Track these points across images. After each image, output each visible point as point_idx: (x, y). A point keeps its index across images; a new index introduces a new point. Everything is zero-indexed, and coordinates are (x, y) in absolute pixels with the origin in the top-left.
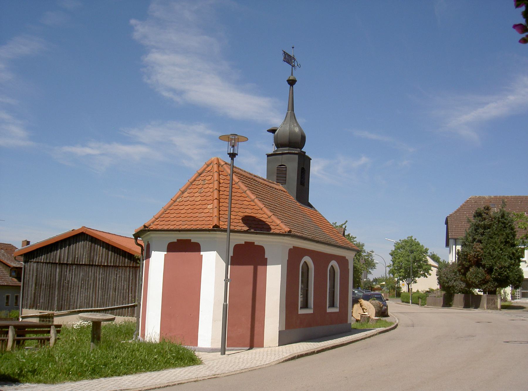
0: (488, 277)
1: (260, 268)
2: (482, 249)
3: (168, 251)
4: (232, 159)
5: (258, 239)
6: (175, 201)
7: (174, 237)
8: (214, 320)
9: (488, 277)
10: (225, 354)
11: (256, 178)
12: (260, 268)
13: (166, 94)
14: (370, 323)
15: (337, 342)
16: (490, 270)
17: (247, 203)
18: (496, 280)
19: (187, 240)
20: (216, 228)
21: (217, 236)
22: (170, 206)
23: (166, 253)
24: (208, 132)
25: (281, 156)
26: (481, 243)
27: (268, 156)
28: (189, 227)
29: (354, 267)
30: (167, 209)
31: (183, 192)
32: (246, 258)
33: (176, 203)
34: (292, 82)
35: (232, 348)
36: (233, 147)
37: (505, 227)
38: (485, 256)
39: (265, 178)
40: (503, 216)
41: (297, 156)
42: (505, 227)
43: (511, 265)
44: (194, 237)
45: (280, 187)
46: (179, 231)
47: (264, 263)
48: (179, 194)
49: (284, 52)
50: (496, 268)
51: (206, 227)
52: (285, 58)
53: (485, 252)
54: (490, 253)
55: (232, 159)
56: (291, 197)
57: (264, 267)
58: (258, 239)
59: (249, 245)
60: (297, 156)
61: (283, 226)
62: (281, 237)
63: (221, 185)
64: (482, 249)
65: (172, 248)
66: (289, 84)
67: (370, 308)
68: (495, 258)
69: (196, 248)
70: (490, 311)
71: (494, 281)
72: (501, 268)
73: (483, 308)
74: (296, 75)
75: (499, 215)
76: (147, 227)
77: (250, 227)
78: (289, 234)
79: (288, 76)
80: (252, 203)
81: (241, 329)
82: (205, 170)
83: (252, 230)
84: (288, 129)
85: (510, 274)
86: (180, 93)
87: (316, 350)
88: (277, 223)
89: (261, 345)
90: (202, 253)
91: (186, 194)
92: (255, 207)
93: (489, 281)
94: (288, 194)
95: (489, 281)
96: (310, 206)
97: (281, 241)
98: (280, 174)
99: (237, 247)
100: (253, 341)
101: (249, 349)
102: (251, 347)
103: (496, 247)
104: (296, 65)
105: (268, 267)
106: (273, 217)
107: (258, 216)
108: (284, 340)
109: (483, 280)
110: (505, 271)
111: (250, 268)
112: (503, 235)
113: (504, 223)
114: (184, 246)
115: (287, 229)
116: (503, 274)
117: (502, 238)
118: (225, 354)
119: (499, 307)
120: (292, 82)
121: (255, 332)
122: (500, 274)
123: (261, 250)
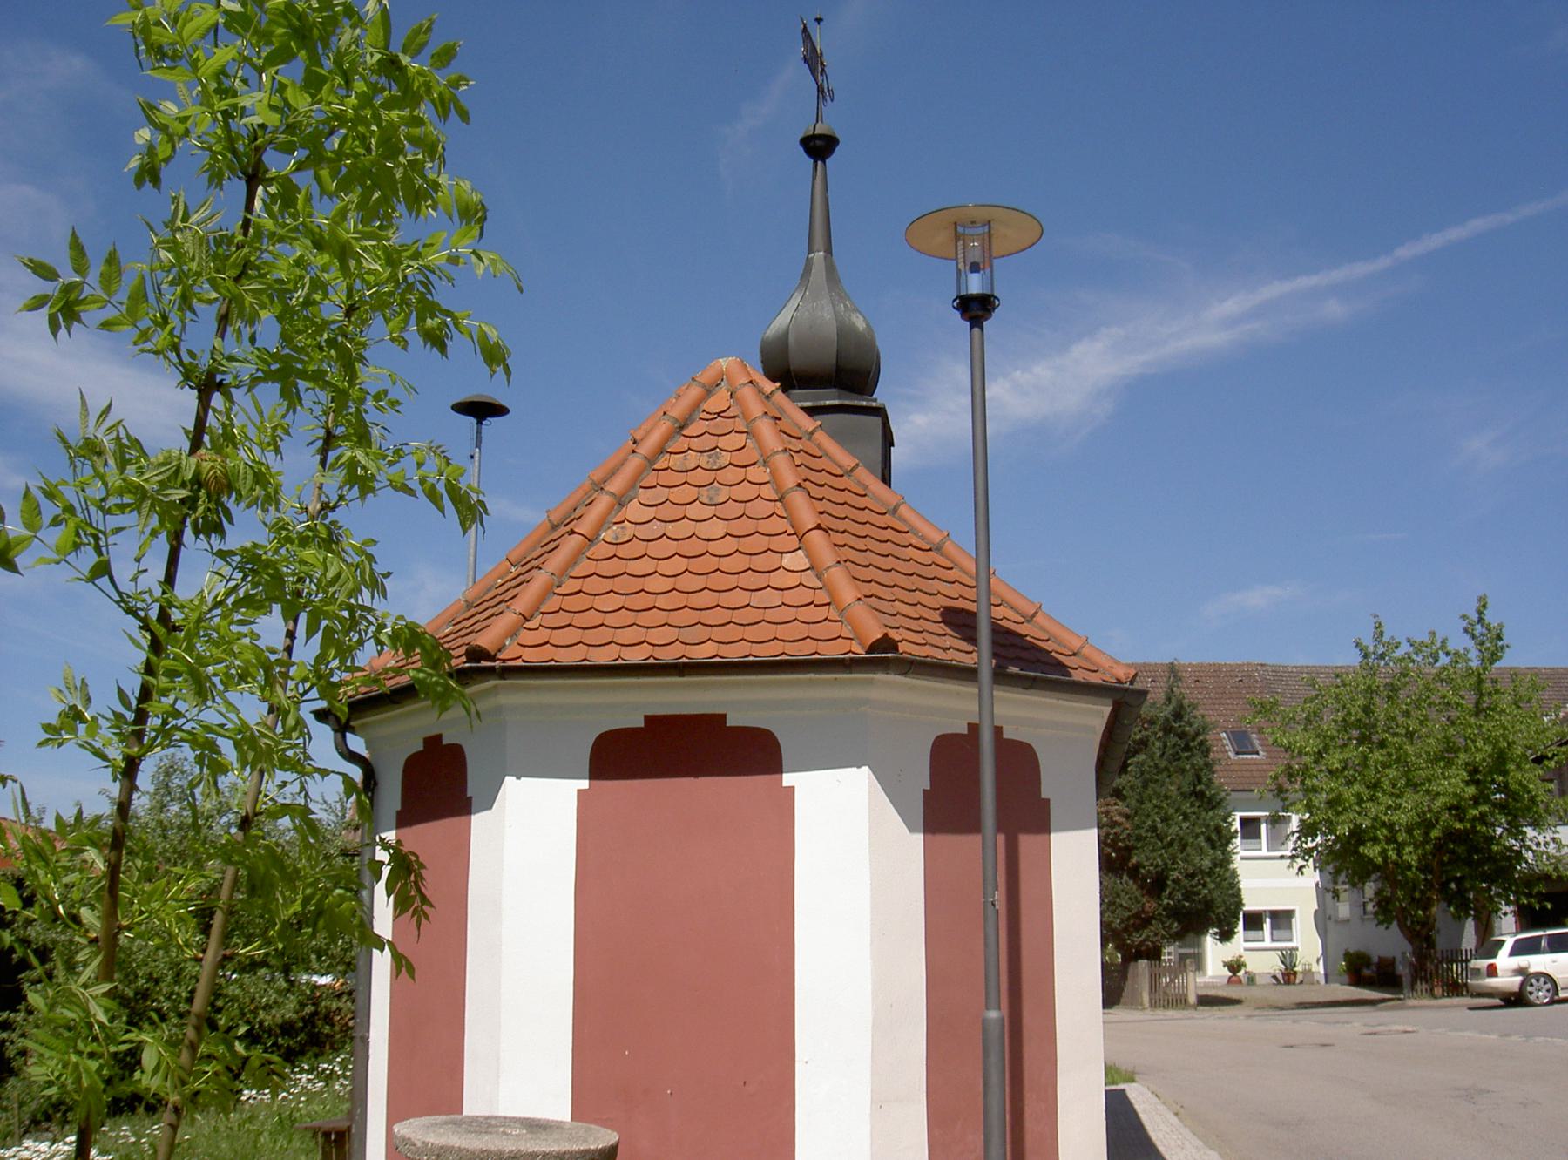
0: (1150, 905)
1: (1026, 841)
2: (1127, 817)
3: (594, 775)
7: (629, 706)
8: (879, 1103)
9: (1150, 905)
12: (1026, 841)
16: (1157, 885)
18: (1175, 913)
19: (696, 716)
20: (883, 656)
21: (875, 694)
23: (584, 784)
26: (1124, 798)
29: (208, 936)
33: (600, 550)
34: (819, 147)
37: (1187, 748)
38: (1139, 838)
40: (1178, 715)
42: (1187, 748)
43: (1215, 865)
44: (740, 703)
50: (1175, 874)
51: (832, 651)
53: (1138, 827)
54: (1154, 829)
57: (1040, 838)
64: (1127, 817)
65: (616, 757)
68: (1171, 844)
69: (757, 753)
70: (1160, 1012)
71: (1168, 917)
72: (1191, 876)
73: (1135, 1004)
75: (1167, 712)
76: (493, 659)
85: (1216, 894)
90: (788, 779)
91: (634, 510)
93: (1153, 918)
95: (1153, 918)
103: (1171, 811)
105: (1055, 837)
109: (1136, 916)
110: (1204, 886)
112: (1183, 771)
113: (1182, 735)
114: (685, 747)
116: (1198, 894)
117: (1185, 782)
119: (1192, 999)
120: (819, 147)
122: (1187, 897)
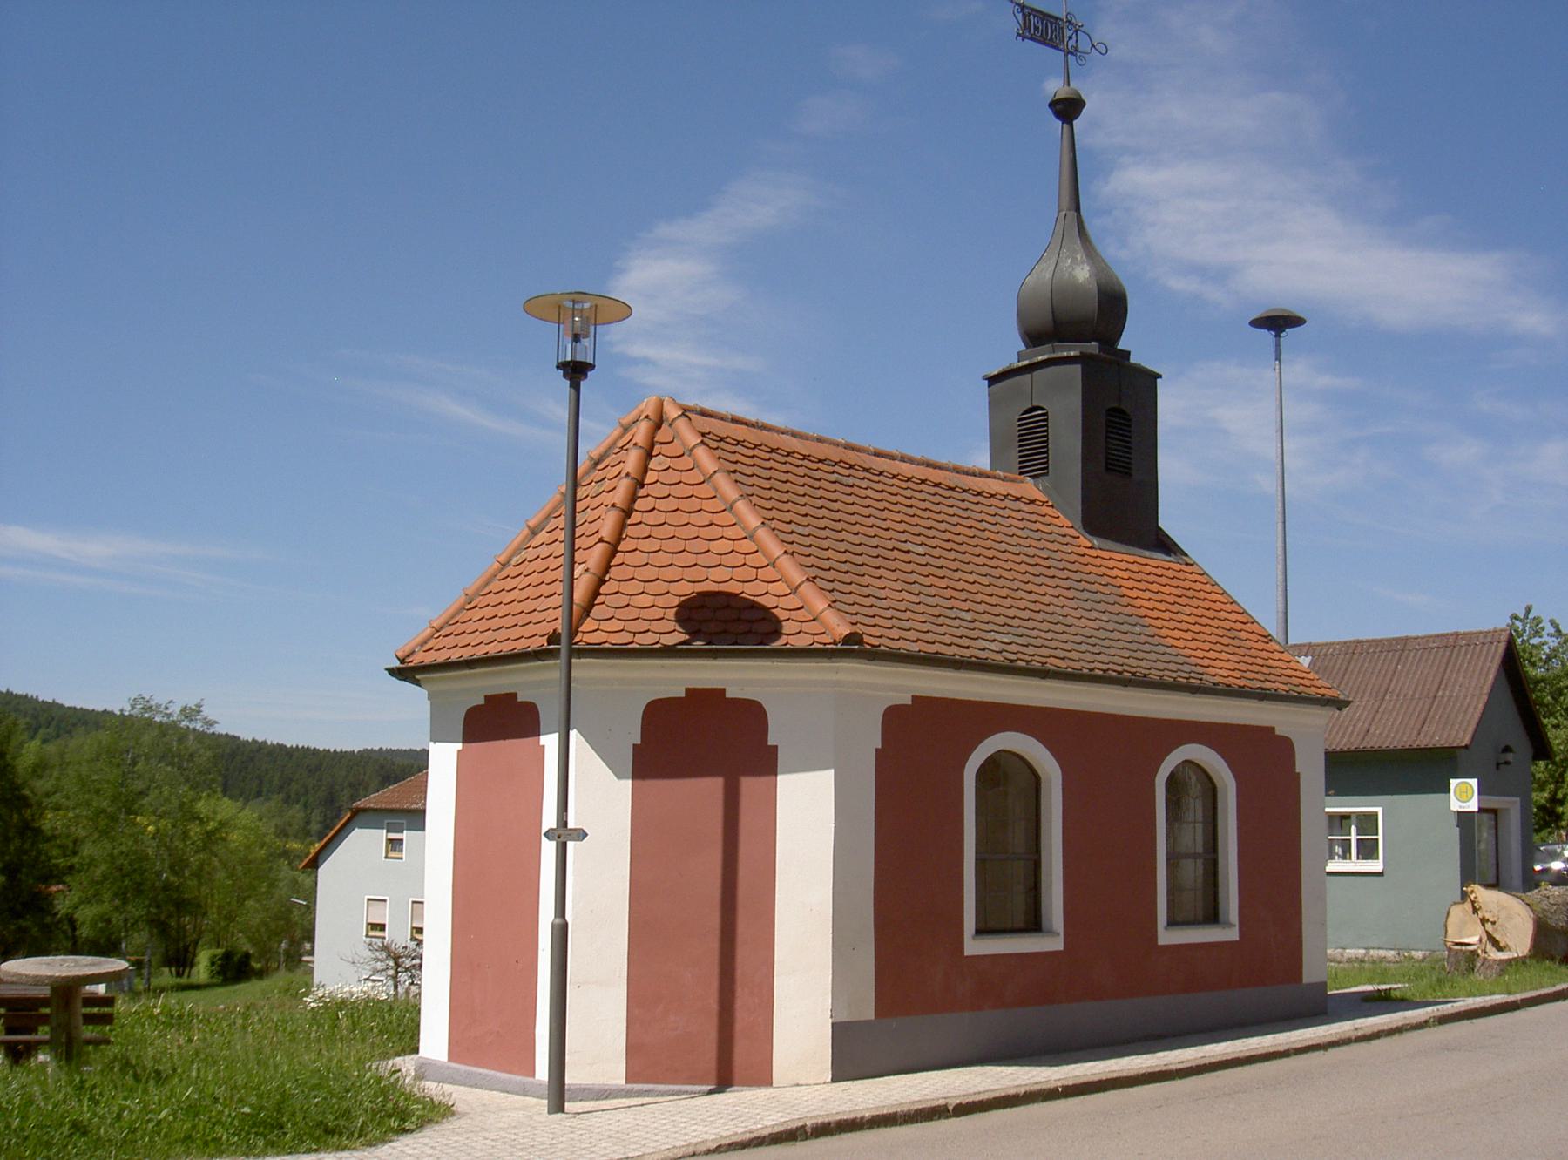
1: (748, 784)
4: (575, 386)
5: (736, 677)
6: (504, 566)
10: (562, 1110)
11: (852, 457)
12: (748, 784)
13: (1178, 284)
14: (1478, 976)
15: (1115, 1068)
17: (728, 546)
22: (487, 583)
23: (459, 746)
24: (1324, 381)
25: (1028, 376)
27: (993, 380)
28: (506, 648)
30: (477, 594)
31: (534, 532)
32: (701, 749)
35: (651, 1086)
36: (576, 338)
39: (983, 461)
41: (1077, 368)
45: (1029, 487)
46: (470, 663)
47: (766, 763)
48: (519, 539)
49: (1023, 7)
52: (1026, 26)
55: (575, 386)
56: (1063, 520)
58: (736, 677)
59: (704, 700)
60: (1077, 368)
61: (831, 618)
62: (826, 664)
63: (642, 492)
66: (1058, 115)
67: (1510, 917)
74: (1080, 86)
77: (694, 634)
78: (852, 647)
79: (1054, 87)
80: (747, 546)
81: (703, 1020)
82: (614, 444)
83: (698, 644)
84: (1048, 275)
86: (1220, 275)
87: (952, 1103)
88: (811, 612)
89: (763, 1077)
92: (759, 559)
94: (1049, 511)
96: (1165, 545)
97: (815, 676)
98: (1028, 445)
99: (657, 713)
100: (731, 1058)
101: (711, 1092)
102: (724, 1081)
104: (1084, 45)
106: (807, 590)
107: (750, 591)
108: (853, 1054)
111: (710, 788)
115: (840, 628)
118: (562, 1110)
121: (739, 1026)
123: (752, 715)
